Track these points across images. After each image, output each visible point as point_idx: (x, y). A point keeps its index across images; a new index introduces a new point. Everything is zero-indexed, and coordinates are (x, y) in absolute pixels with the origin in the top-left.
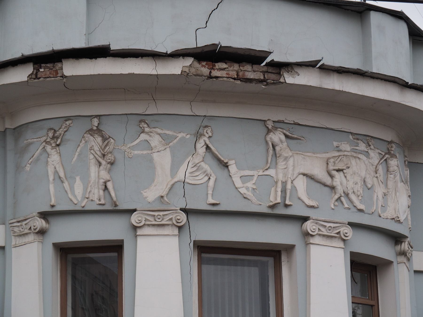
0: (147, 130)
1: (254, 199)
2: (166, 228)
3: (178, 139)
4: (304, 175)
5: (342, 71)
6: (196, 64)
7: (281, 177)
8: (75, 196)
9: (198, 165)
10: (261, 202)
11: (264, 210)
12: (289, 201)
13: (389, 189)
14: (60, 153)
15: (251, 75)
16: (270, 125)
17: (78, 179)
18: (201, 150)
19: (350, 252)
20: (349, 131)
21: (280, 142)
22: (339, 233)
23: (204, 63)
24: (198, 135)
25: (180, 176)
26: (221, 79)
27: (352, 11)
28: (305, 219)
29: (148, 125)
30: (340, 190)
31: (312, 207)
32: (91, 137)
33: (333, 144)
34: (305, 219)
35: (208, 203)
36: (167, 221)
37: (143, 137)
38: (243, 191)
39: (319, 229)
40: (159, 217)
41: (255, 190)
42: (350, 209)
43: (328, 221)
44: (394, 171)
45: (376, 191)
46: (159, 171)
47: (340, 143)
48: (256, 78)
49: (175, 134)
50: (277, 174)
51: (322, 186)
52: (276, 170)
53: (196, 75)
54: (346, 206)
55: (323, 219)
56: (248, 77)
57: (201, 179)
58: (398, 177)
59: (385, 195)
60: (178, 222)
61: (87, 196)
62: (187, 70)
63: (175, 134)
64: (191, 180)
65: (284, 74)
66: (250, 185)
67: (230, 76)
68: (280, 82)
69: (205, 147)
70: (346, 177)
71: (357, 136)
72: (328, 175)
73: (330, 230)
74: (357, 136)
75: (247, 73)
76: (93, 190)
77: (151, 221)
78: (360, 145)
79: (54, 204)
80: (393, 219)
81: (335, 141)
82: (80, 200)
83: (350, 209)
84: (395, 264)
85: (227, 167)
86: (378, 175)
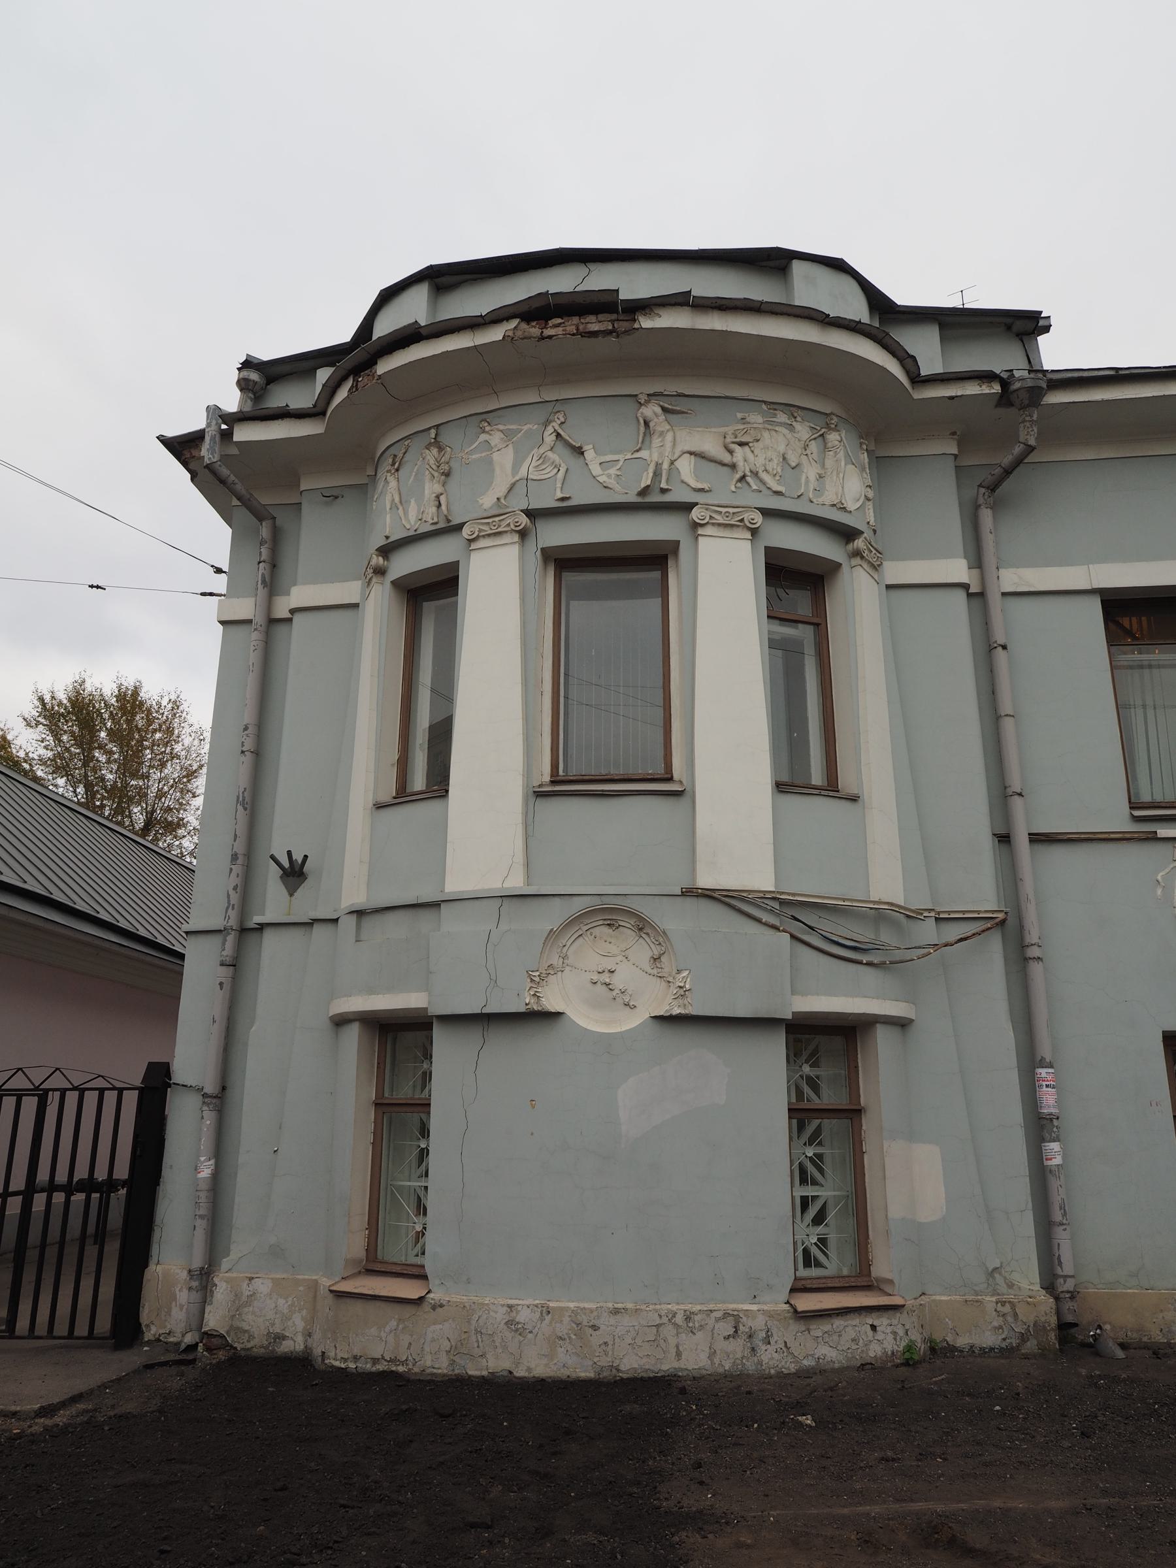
0: (487, 429)
1: (618, 488)
2: (505, 536)
3: (523, 432)
4: (691, 453)
5: (724, 307)
6: (524, 326)
7: (655, 457)
8: (409, 522)
9: (544, 456)
10: (628, 490)
11: (632, 498)
12: (666, 484)
13: (827, 469)
14: (398, 478)
15: (595, 327)
16: (643, 398)
17: (413, 501)
18: (550, 439)
19: (765, 547)
20: (761, 399)
21: (654, 416)
22: (742, 520)
23: (534, 324)
24: (547, 423)
25: (523, 472)
26: (555, 338)
27: (771, 268)
28: (692, 505)
29: (488, 422)
30: (743, 467)
31: (701, 490)
32: (427, 451)
33: (736, 416)
34: (692, 505)
35: (556, 498)
36: (505, 527)
37: (483, 437)
38: (601, 479)
39: (710, 516)
40: (494, 523)
41: (620, 477)
42: (761, 491)
43: (723, 505)
44: (833, 447)
45: (805, 471)
46: (498, 471)
47: (747, 415)
48: (603, 329)
49: (520, 427)
50: (651, 455)
51: (720, 467)
52: (650, 452)
53: (522, 339)
54: (755, 487)
55: (716, 502)
56: (591, 330)
57: (549, 472)
58: (841, 455)
59: (820, 477)
60: (516, 526)
61: (420, 518)
62: (511, 334)
63: (520, 427)
64: (536, 475)
65: (640, 318)
66: (613, 471)
67: (567, 332)
68: (634, 329)
69: (554, 434)
70: (753, 452)
71: (774, 406)
72: (725, 450)
73: (727, 517)
74: (774, 406)
75: (590, 325)
76: (427, 511)
77: (486, 531)
78: (779, 416)
79: (388, 535)
80: (834, 505)
81: (740, 412)
82: (413, 524)
83: (761, 491)
84: (845, 568)
85: (582, 453)
86: (808, 452)
